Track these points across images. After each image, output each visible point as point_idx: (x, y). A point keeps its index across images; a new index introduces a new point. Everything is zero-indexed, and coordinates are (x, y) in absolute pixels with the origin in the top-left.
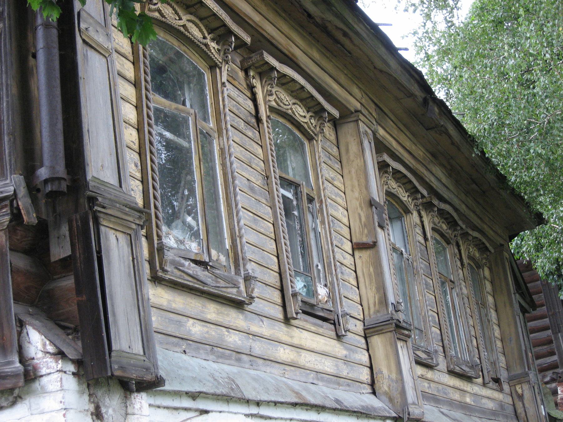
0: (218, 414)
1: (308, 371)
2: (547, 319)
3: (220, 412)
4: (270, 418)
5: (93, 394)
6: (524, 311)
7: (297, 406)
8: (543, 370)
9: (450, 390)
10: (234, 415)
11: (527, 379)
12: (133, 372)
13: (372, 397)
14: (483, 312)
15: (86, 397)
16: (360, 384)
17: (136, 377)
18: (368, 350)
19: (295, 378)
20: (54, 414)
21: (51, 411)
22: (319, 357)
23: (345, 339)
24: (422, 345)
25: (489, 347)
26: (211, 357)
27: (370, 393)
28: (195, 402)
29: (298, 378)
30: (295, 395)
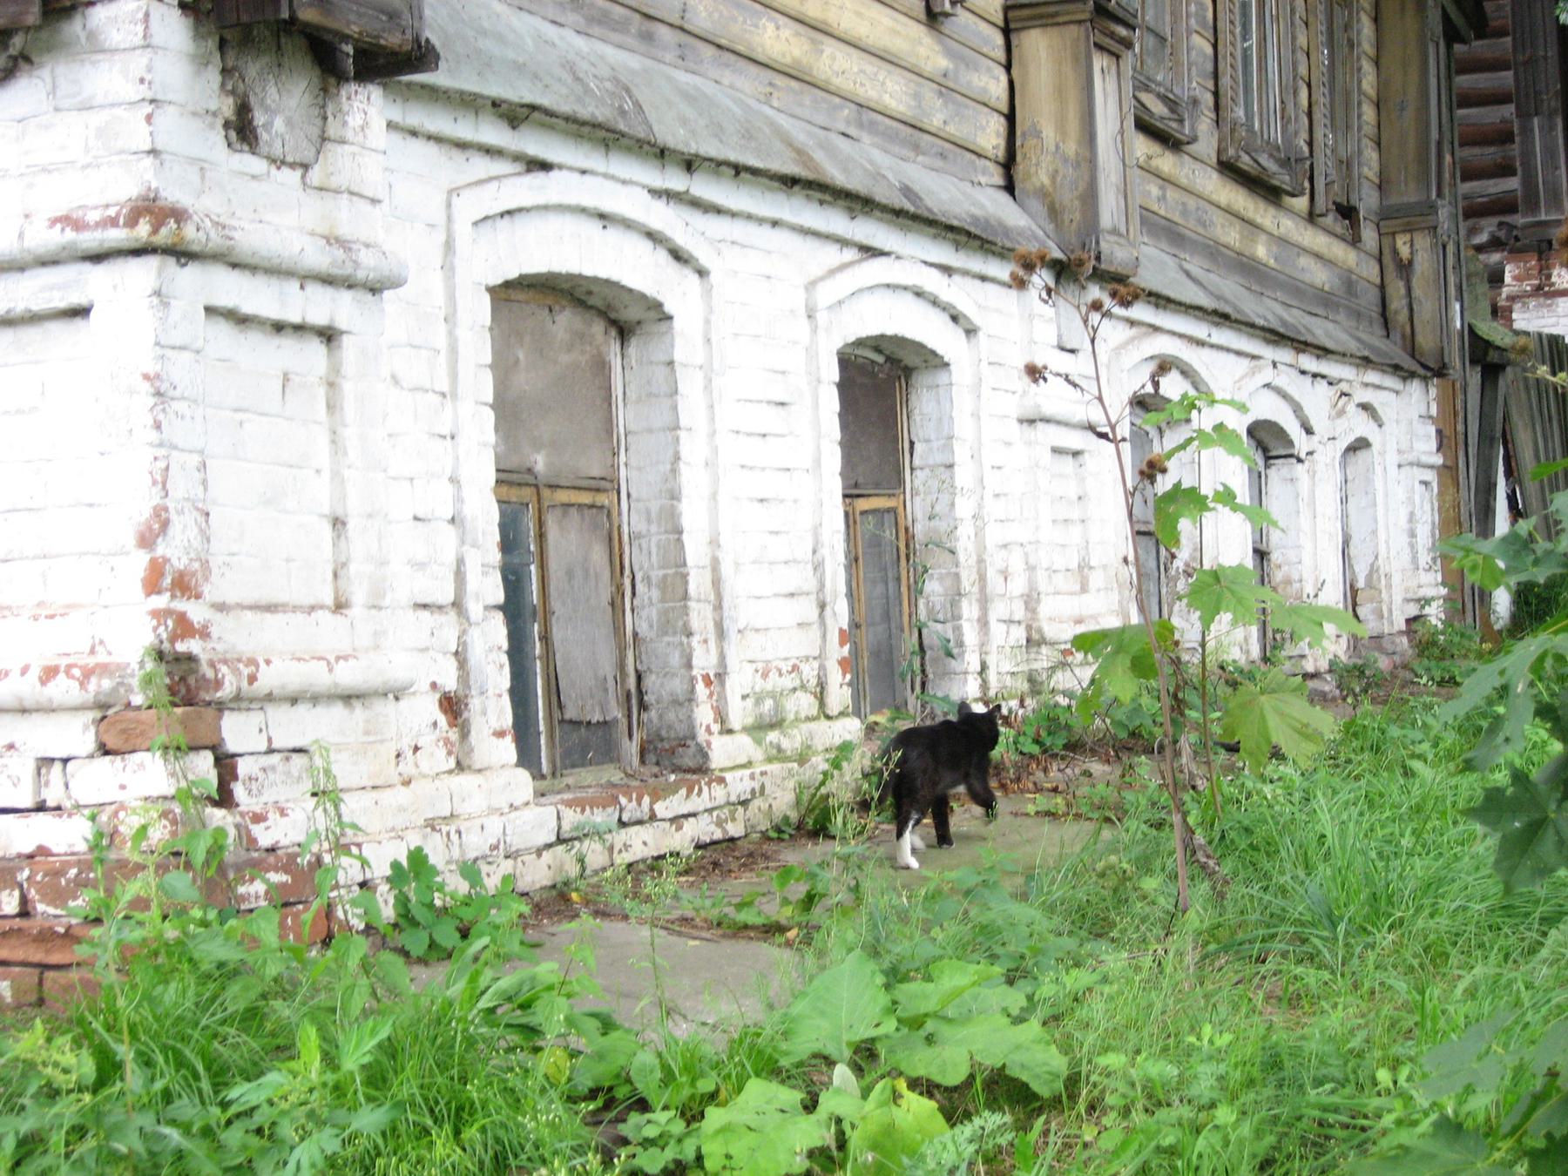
0: (576, 176)
1: (837, 100)
2: (1510, 74)
3: (584, 172)
4: (719, 210)
5: (234, 68)
6: (1452, 35)
7: (796, 188)
8: (1474, 212)
9: (1218, 218)
10: (619, 186)
11: (1430, 220)
12: (352, 17)
13: (1004, 198)
14: (1340, 16)
15: (213, 76)
16: (974, 157)
17: (360, 33)
18: (1008, 67)
19: (798, 111)
20: (118, 111)
21: (113, 105)
22: (871, 66)
23: (948, 26)
24: (1159, 78)
25: (1340, 123)
26: (572, 18)
27: (999, 187)
28: (516, 134)
29: (806, 114)
30: (793, 155)
